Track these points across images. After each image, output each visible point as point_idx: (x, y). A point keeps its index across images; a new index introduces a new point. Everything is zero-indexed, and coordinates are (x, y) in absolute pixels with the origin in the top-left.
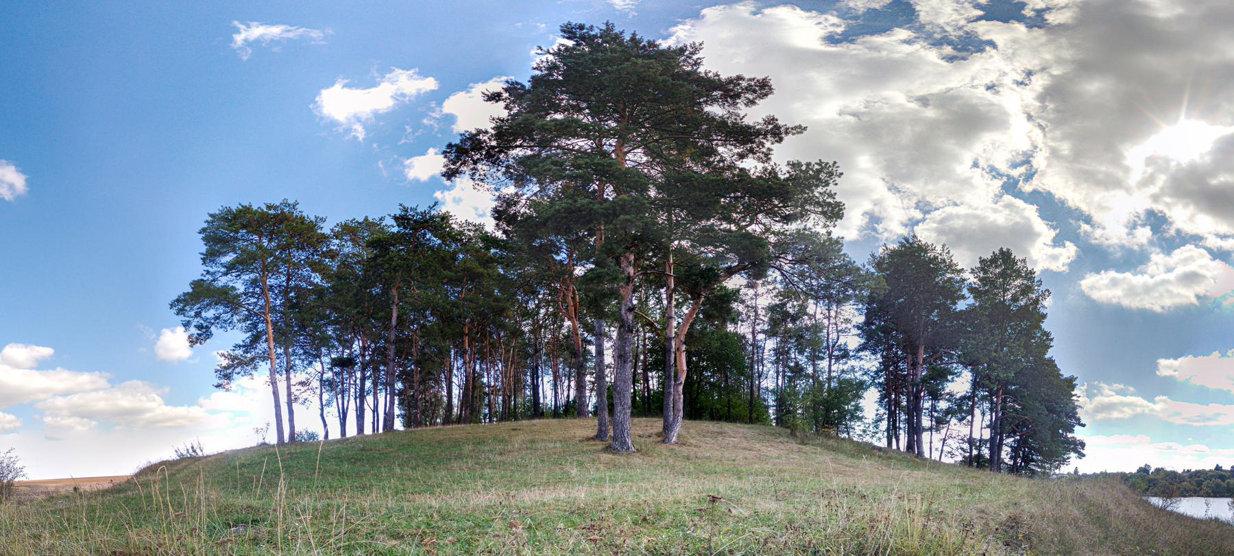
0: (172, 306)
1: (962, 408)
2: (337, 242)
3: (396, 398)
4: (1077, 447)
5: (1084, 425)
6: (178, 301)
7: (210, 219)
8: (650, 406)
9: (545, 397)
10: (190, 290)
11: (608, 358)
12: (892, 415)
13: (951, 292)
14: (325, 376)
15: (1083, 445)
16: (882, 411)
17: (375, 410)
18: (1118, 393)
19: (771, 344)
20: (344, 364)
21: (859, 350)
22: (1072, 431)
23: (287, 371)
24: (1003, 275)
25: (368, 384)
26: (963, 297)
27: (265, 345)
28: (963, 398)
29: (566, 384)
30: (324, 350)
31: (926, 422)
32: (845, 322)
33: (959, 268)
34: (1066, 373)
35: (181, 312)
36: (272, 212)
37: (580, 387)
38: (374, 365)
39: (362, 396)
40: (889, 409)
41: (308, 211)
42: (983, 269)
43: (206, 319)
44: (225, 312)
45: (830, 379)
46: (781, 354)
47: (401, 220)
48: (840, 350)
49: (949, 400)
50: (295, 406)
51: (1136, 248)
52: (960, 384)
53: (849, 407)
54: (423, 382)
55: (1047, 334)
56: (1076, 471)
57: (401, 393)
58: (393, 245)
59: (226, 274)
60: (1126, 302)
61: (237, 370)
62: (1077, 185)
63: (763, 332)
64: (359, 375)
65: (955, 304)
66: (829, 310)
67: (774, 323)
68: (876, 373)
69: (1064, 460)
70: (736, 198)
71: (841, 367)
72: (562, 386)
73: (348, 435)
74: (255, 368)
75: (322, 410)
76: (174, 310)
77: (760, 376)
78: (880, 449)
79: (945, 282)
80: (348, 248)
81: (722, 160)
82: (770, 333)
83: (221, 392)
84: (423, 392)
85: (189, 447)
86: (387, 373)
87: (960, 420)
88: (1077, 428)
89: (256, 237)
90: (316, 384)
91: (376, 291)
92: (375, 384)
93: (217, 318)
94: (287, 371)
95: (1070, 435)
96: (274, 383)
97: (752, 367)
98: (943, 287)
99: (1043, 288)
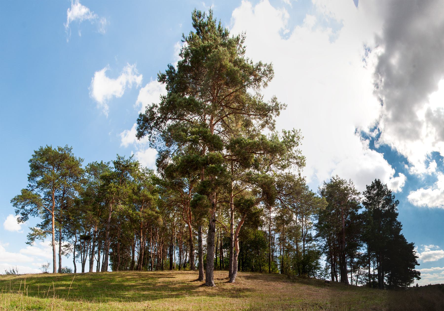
0: (12, 201)
1: (364, 261)
2: (87, 174)
3: (109, 256)
4: (417, 275)
5: (419, 265)
6: (15, 199)
7: (34, 154)
8: (224, 265)
9: (175, 260)
10: (21, 194)
11: (204, 242)
12: (333, 266)
13: (355, 206)
14: (77, 243)
15: (419, 273)
16: (329, 264)
17: (98, 261)
18: (432, 249)
19: (277, 236)
20: (86, 238)
21: (316, 237)
22: (414, 268)
23: (60, 240)
24: (378, 194)
25: (96, 249)
26: (361, 207)
27: (51, 226)
28: (365, 256)
29: (185, 254)
30: (77, 231)
31: (349, 268)
32: (310, 224)
33: (358, 192)
34: (409, 241)
35: (15, 205)
36: (60, 152)
37: (191, 256)
38: (99, 240)
39: (92, 254)
40: (332, 263)
41: (76, 154)
42: (368, 192)
43: (26, 210)
44: (35, 208)
45: (304, 251)
46: (282, 240)
47: (117, 164)
48: (308, 237)
49: (358, 258)
50: (62, 256)
51: (430, 174)
52: (363, 250)
53: (314, 264)
54: (122, 249)
55: (399, 223)
56: (417, 285)
57: (111, 254)
58: (112, 179)
59: (37, 187)
60: (430, 205)
61: (37, 237)
62: (407, 158)
63: (274, 230)
64: (92, 244)
65: (357, 211)
66: (302, 218)
67: (278, 225)
68: (325, 247)
69: (412, 281)
70: (261, 154)
71: (309, 245)
72: (183, 255)
73: (85, 272)
74: (45, 237)
75: (74, 259)
76: (12, 204)
77: (273, 251)
78: (328, 282)
79: (352, 200)
80: (92, 179)
81: (254, 130)
82: (277, 231)
83: (29, 246)
84: (122, 254)
85: (12, 270)
86: (105, 244)
87: (364, 266)
88: (416, 266)
89: (51, 167)
90: (72, 247)
91: (103, 204)
92: (99, 249)
93: (31, 210)
94: (60, 240)
95: (413, 270)
96: (53, 245)
97: (269, 247)
98: (352, 203)
99: (395, 200)
